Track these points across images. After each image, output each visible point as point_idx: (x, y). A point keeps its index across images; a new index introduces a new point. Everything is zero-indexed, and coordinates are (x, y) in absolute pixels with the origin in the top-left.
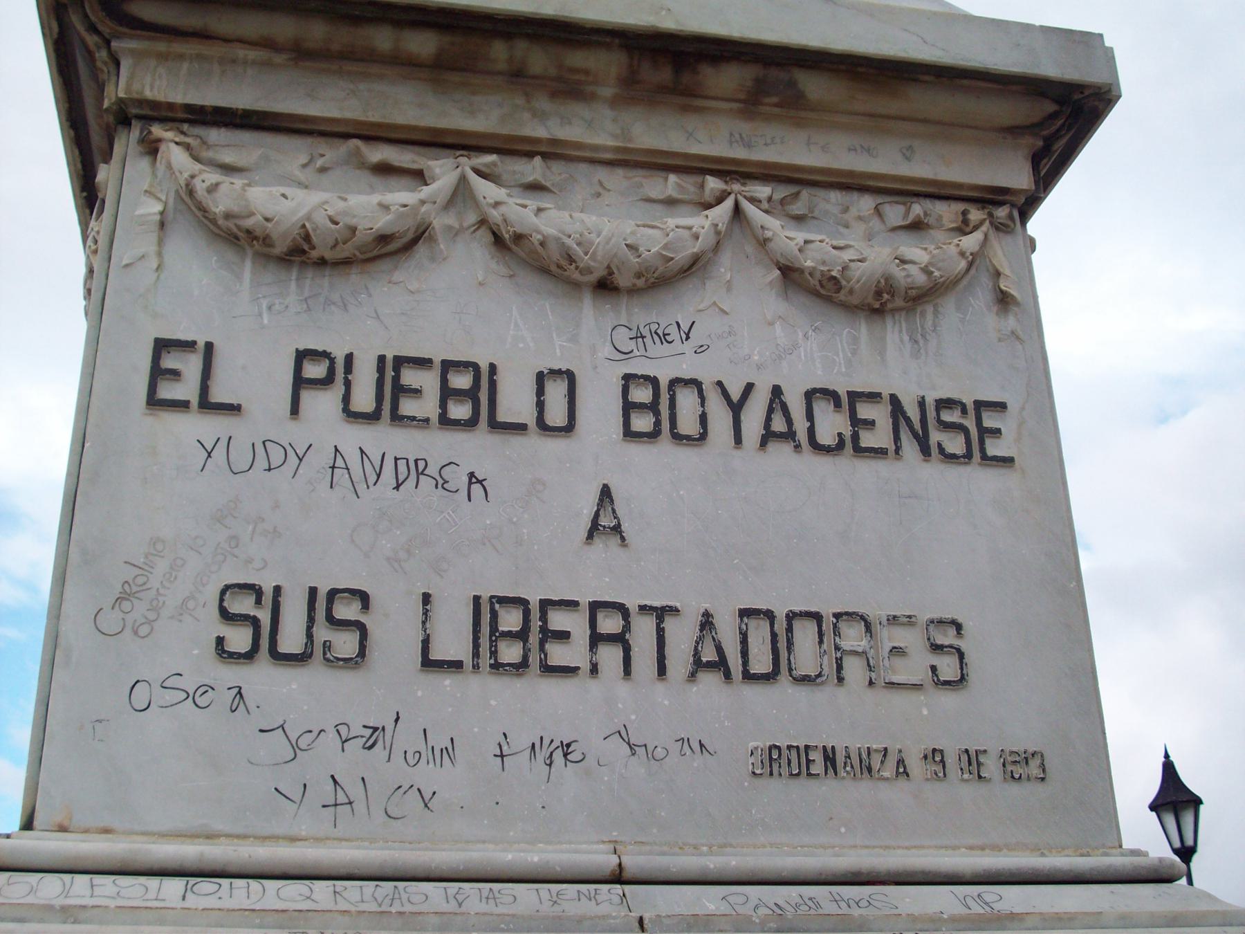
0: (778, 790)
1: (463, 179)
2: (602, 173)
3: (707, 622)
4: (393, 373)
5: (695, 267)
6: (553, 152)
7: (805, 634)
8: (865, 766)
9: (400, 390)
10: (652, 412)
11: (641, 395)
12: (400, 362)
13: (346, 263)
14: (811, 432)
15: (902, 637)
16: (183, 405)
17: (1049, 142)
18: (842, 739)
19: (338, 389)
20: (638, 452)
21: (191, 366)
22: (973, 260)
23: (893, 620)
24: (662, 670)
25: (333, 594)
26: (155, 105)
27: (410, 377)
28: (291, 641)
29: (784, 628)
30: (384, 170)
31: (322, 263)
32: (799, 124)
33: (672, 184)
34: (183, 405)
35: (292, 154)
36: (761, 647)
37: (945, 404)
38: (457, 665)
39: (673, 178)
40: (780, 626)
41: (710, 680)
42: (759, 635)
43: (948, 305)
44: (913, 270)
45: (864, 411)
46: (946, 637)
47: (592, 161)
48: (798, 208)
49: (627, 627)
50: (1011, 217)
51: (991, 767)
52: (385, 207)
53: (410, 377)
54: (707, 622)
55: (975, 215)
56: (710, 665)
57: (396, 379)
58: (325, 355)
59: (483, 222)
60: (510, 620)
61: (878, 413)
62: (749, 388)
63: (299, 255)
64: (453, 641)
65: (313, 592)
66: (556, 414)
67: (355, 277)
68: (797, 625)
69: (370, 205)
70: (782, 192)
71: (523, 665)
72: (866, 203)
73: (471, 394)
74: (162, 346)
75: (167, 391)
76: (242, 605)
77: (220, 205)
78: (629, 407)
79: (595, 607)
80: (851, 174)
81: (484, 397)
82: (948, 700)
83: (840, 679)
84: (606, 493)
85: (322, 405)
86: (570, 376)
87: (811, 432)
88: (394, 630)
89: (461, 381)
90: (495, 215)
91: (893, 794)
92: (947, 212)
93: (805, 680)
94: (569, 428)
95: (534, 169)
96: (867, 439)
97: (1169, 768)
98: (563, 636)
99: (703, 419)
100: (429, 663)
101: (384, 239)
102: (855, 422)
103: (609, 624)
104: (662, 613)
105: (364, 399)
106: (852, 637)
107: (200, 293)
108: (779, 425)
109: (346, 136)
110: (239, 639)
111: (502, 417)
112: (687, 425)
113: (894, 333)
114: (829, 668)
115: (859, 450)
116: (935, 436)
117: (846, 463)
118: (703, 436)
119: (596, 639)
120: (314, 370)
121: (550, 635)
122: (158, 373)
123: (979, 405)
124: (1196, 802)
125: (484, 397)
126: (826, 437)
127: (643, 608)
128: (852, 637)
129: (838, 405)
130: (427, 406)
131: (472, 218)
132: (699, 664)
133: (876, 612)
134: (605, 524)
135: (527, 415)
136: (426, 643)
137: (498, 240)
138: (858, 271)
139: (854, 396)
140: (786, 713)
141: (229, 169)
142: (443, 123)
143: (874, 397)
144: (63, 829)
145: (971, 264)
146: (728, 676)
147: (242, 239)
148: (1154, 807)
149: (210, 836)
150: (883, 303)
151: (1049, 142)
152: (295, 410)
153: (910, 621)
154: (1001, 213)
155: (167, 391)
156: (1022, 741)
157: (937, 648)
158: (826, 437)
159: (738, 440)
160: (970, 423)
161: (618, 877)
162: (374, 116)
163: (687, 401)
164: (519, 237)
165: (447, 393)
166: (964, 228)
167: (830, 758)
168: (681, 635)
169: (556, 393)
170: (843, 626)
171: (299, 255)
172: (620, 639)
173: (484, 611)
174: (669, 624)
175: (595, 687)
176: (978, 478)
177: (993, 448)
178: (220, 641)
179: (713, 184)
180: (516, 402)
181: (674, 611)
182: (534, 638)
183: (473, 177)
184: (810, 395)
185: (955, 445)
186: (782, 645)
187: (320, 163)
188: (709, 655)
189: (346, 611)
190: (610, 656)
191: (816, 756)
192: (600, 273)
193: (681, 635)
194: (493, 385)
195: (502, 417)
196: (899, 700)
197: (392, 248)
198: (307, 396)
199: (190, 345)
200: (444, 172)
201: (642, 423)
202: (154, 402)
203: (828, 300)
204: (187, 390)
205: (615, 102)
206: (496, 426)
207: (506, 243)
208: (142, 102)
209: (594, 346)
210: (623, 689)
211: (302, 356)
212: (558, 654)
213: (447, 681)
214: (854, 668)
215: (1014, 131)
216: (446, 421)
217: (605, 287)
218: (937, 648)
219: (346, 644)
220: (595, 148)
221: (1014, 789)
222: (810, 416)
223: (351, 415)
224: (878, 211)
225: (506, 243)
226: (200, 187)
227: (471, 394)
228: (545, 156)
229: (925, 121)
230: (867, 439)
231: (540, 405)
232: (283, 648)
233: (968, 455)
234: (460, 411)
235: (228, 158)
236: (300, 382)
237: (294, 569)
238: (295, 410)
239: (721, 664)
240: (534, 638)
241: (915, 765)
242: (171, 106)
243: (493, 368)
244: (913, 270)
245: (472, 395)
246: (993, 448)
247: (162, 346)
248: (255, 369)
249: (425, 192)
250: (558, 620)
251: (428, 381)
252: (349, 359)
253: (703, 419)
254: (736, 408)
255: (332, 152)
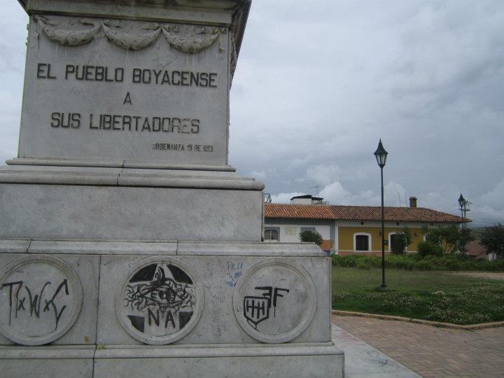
0: (158, 152)
1: (101, 26)
2: (133, 23)
3: (146, 120)
4: (86, 68)
5: (151, 45)
6: (121, 18)
7: (166, 122)
8: (175, 148)
9: (88, 73)
10: (139, 76)
11: (137, 73)
12: (88, 67)
13: (77, 46)
14: (173, 81)
15: (187, 123)
16: (44, 77)
17: (236, 12)
18: (171, 142)
19: (75, 73)
20: (135, 85)
21: (46, 69)
22: (214, 42)
23: (185, 119)
24: (137, 129)
25: (73, 115)
26: (35, 11)
27: (90, 70)
28: (66, 123)
29: (162, 121)
30: (85, 24)
31: (72, 46)
32: (177, 10)
33: (147, 25)
34: (44, 77)
35: (65, 21)
36: (158, 124)
37: (203, 74)
38: (97, 128)
39: (148, 24)
40: (161, 121)
41: (146, 131)
42: (157, 122)
43: (208, 51)
44: (198, 45)
45: (185, 76)
46: (196, 123)
47: (131, 20)
48: (176, 30)
49: (130, 121)
50: (225, 30)
51: (201, 149)
52: (83, 34)
53: (90, 70)
54: (146, 120)
55: (217, 30)
56: (146, 128)
57: (87, 71)
58: (72, 66)
59: (106, 36)
60: (108, 119)
61: (188, 77)
62: (160, 71)
63: (66, 44)
64: (96, 123)
65: (70, 114)
66: (119, 78)
67: (79, 49)
68: (165, 121)
69: (80, 32)
70: (172, 26)
71: (109, 128)
72: (193, 27)
73: (102, 74)
74: (40, 65)
75: (41, 75)
76: (56, 117)
77: (49, 34)
78: (134, 76)
79: (124, 117)
80: (188, 21)
81: (104, 74)
82: (194, 135)
83: (172, 131)
84: (128, 94)
85: (72, 76)
86: (123, 70)
87: (173, 81)
88: (85, 121)
89: (100, 71)
90: (107, 34)
91: (180, 153)
92: (210, 29)
93: (166, 131)
94: (122, 80)
95: (117, 23)
96: (185, 82)
97: (380, 144)
98: (118, 122)
99: (150, 78)
100: (91, 127)
101: (83, 41)
102: (183, 78)
103: (127, 120)
104: (137, 118)
105: (80, 75)
106: (176, 123)
107: (48, 54)
108: (166, 79)
109: (77, 16)
110: (56, 123)
111: (108, 78)
112: (147, 79)
113: (194, 58)
114: (170, 129)
115: (182, 84)
116: (200, 81)
117: (180, 87)
118: (149, 82)
119: (124, 123)
120: (70, 69)
121: (115, 122)
122: (39, 71)
123: (211, 74)
124: (386, 153)
125: (104, 74)
126: (176, 82)
127: (134, 117)
128: (176, 123)
129: (179, 75)
130: (93, 76)
131: (103, 35)
132: (144, 128)
133: (181, 118)
134: (128, 100)
135: (113, 78)
136: (91, 124)
137: (109, 40)
138: (185, 45)
139: (183, 73)
140: (162, 137)
141: (53, 25)
142: (97, 13)
143: (187, 73)
144: (24, 157)
145: (213, 43)
146: (150, 130)
147: (55, 41)
148: (375, 154)
149: (50, 159)
150: (191, 52)
151: (236, 12)
152: (66, 78)
153: (188, 120)
154: (223, 29)
155: (41, 75)
156: (209, 143)
157: (193, 125)
158: (176, 82)
159: (157, 82)
160: (208, 79)
161: (123, 167)
162: (82, 12)
163: (147, 74)
164: (112, 39)
165: (97, 73)
166: (214, 33)
167: (168, 146)
168: (141, 122)
169: (119, 73)
170: (174, 121)
171: (66, 44)
172: (129, 123)
173: (102, 118)
174: (139, 120)
175: (124, 132)
176: (209, 91)
177: (213, 84)
178: (52, 124)
179: (156, 25)
180: (111, 75)
181: (140, 117)
182: (112, 122)
183: (103, 25)
184: (173, 73)
185: (204, 83)
186: (161, 124)
187: (72, 23)
188: (146, 126)
189: (76, 117)
190: (127, 126)
191: (166, 146)
192: (129, 47)
193: (141, 122)
194: (106, 72)
195: (108, 78)
196: (185, 135)
197: (86, 42)
198: (69, 75)
199: (45, 65)
200: (97, 24)
201: (137, 79)
202: (39, 77)
203: (181, 51)
204: (45, 74)
205: (135, 6)
206: (106, 80)
207: (110, 40)
208: (33, 10)
209: (130, 63)
210: (129, 132)
211: (68, 66)
212: (117, 126)
213: (95, 131)
214: (176, 129)
215: (227, 9)
216: (96, 79)
217: (131, 49)
218: (193, 125)
219: (76, 124)
220: (131, 17)
221: (206, 153)
222: (173, 77)
223: (77, 78)
224: (195, 30)
225: (110, 40)
226: (45, 30)
227: (102, 74)
228: (120, 19)
229: (207, 8)
230: (185, 82)
231: (116, 76)
232: (168, 121)
233: (206, 85)
234: (99, 77)
235: (52, 22)
236: (67, 72)
237: (65, 110)
238: (66, 78)
239: (149, 128)
240: (112, 122)
241: (186, 147)
242: (39, 11)
243: (107, 68)
244: (198, 45)
245: (102, 74)
246: (213, 84)
247: (40, 65)
248: (58, 70)
249: (93, 29)
250: (117, 119)
251: (93, 71)
252: (77, 67)
253: (150, 78)
254: (157, 76)
255: (75, 20)
